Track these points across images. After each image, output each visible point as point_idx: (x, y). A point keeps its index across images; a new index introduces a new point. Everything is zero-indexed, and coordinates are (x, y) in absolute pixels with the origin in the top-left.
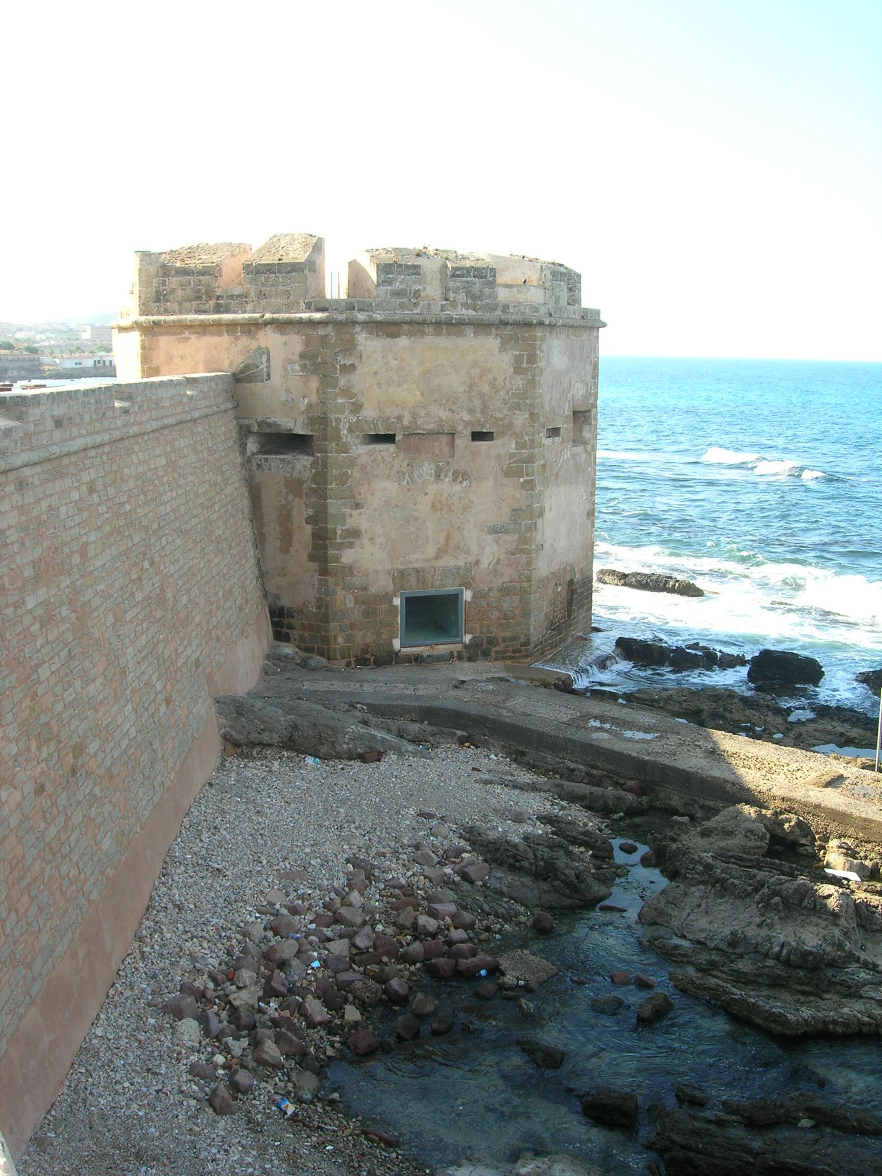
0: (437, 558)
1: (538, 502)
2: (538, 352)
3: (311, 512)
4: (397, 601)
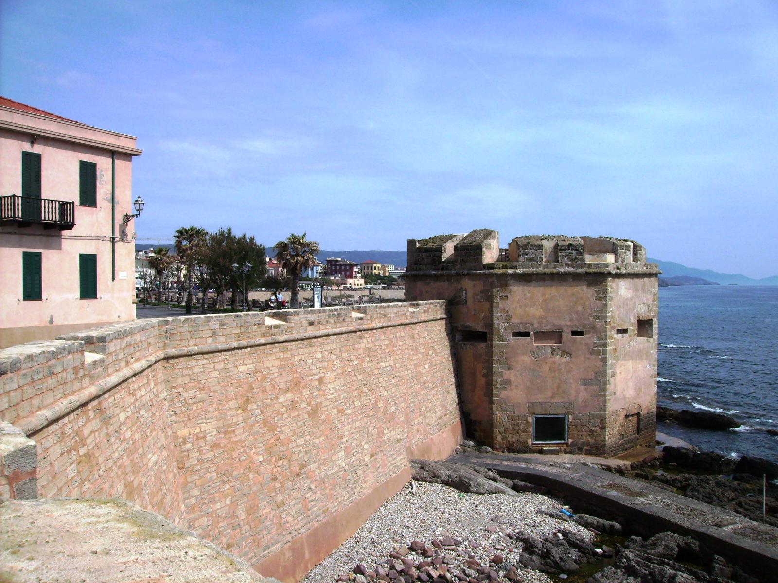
0: (552, 397)
1: (611, 369)
2: (609, 288)
3: (485, 371)
4: (530, 420)
